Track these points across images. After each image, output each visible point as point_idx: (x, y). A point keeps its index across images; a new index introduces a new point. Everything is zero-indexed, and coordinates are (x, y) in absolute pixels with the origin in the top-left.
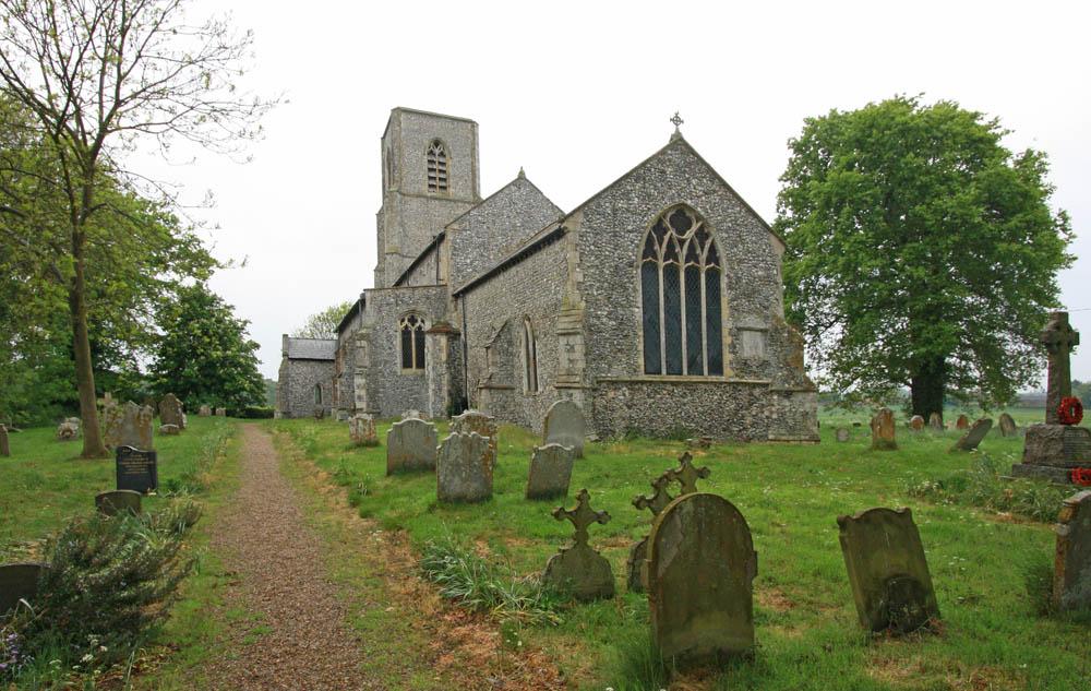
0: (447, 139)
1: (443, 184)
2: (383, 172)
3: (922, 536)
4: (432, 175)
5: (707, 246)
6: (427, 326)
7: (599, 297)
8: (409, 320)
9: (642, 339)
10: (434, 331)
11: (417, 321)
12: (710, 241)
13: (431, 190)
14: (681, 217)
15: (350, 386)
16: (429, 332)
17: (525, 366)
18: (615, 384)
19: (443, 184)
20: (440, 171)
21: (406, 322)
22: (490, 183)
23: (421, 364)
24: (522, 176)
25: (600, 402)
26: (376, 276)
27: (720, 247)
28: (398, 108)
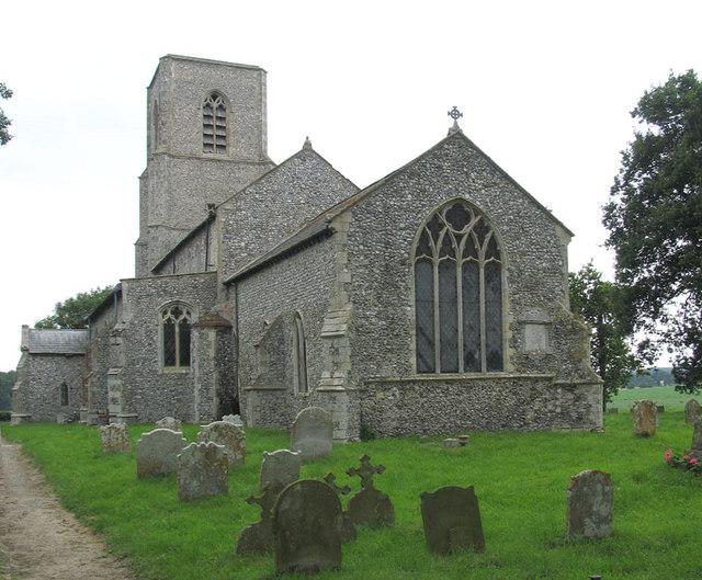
0: (228, 91)
1: (222, 142)
2: (149, 119)
3: (482, 506)
4: (209, 132)
5: (487, 240)
6: (194, 319)
7: (368, 298)
8: (173, 313)
9: (414, 338)
10: (201, 325)
11: (181, 313)
12: (489, 235)
13: (207, 150)
14: (459, 212)
15: (103, 385)
16: (196, 325)
17: (295, 364)
18: (384, 384)
19: (222, 142)
20: (219, 127)
21: (169, 314)
22: (280, 149)
23: (186, 361)
24: (308, 145)
25: (368, 403)
26: (137, 251)
27: (500, 240)
28: (168, 57)
